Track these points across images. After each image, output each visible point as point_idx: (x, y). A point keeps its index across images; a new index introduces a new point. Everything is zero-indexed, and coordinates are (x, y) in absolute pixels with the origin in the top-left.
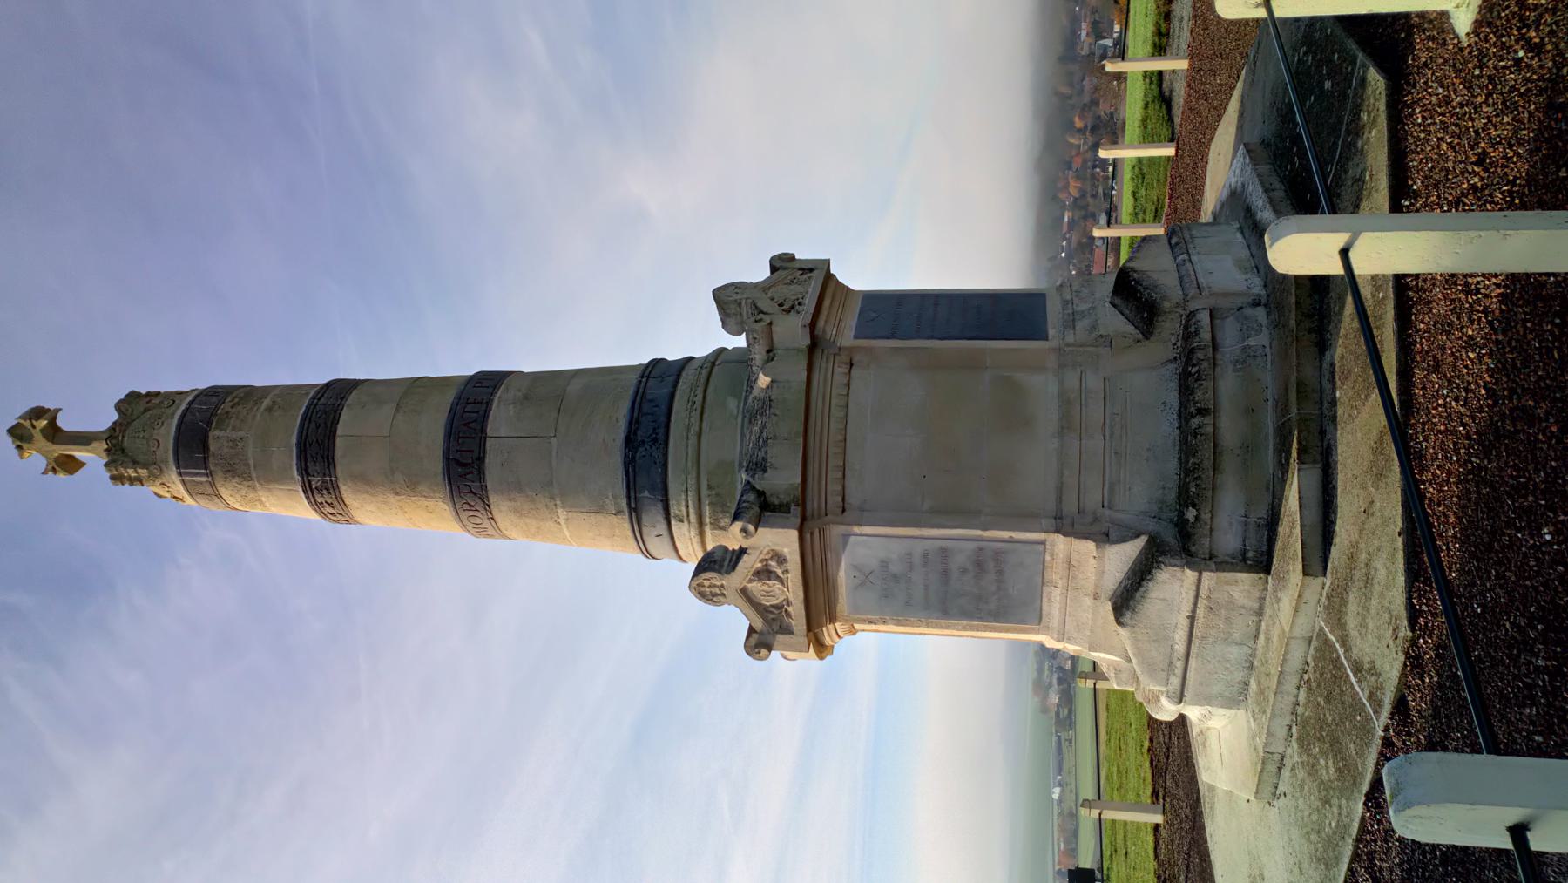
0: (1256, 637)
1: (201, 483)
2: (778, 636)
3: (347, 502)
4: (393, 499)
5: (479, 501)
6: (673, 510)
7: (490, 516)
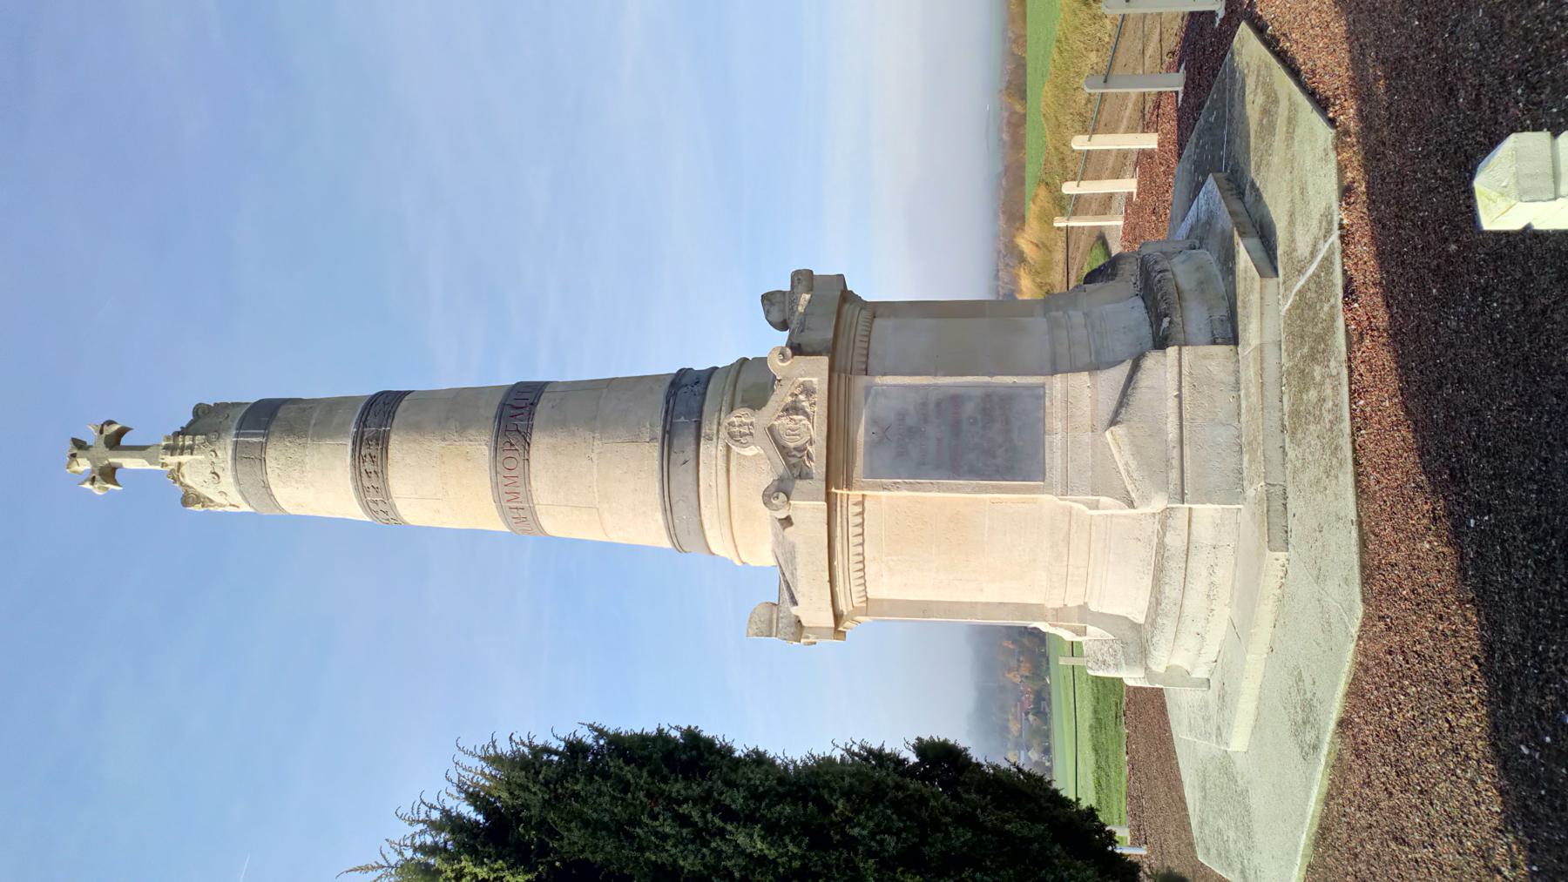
0: (1239, 414)
1: (253, 444)
2: (798, 482)
3: (389, 456)
4: (437, 445)
5: (521, 439)
6: (705, 430)
7: (526, 457)
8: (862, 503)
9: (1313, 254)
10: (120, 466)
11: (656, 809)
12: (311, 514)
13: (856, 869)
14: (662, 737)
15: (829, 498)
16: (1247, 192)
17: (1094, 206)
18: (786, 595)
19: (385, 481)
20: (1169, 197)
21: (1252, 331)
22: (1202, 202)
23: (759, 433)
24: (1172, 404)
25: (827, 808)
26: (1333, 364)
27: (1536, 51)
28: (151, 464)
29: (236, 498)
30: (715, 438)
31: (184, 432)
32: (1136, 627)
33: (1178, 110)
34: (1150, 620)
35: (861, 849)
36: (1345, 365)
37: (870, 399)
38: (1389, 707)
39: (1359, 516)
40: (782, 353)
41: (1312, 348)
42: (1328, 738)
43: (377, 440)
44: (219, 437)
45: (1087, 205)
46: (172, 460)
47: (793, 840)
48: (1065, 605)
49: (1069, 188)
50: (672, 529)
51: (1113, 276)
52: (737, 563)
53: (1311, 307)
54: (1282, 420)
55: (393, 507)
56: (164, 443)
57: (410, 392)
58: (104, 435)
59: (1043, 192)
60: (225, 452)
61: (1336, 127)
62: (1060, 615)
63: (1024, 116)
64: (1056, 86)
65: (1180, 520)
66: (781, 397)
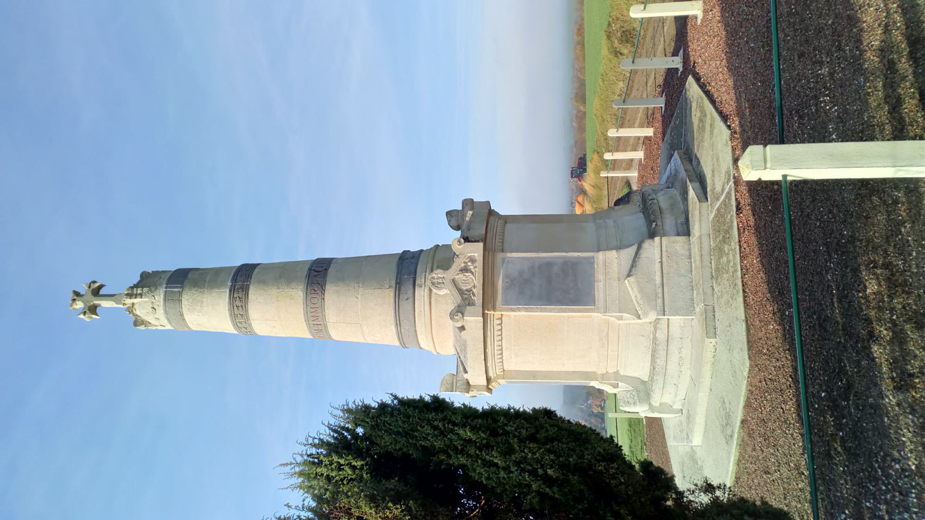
0: (691, 271)
1: (175, 292)
2: (468, 307)
3: (249, 298)
4: (274, 291)
6: (417, 282)
8: (501, 319)
9: (723, 190)
10: (99, 305)
11: (423, 424)
12: (204, 329)
13: (510, 443)
14: (421, 400)
15: (484, 316)
16: (693, 160)
17: (624, 165)
18: (461, 369)
19: (247, 311)
20: (659, 161)
21: (696, 229)
22: (672, 164)
23: (447, 282)
24: (658, 266)
25: (496, 421)
26: (732, 244)
27: (802, 101)
28: (117, 304)
29: (164, 321)
30: (423, 286)
31: (136, 286)
32: (643, 382)
33: (663, 116)
34: (650, 378)
35: (511, 435)
36: (737, 244)
37: (504, 265)
38: (761, 409)
39: (746, 317)
40: (459, 241)
41: (723, 236)
42: (737, 430)
43: (243, 289)
44: (156, 289)
45: (620, 164)
46: (129, 301)
47: (483, 432)
48: (607, 372)
49: (608, 156)
50: (400, 334)
51: (628, 202)
52: (435, 353)
53: (723, 216)
54: (712, 273)
55: (250, 325)
56: (126, 293)
57: (258, 264)
58: (91, 289)
59: (596, 157)
60: (159, 297)
61: (731, 130)
62: (604, 377)
63: (585, 113)
64: (601, 100)
65: (663, 324)
66: (458, 263)
